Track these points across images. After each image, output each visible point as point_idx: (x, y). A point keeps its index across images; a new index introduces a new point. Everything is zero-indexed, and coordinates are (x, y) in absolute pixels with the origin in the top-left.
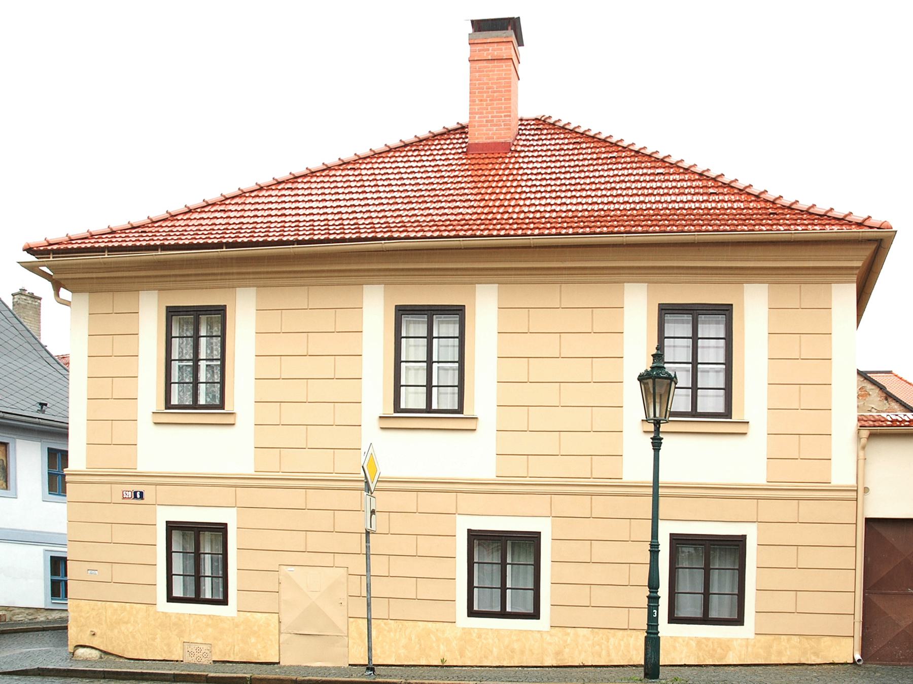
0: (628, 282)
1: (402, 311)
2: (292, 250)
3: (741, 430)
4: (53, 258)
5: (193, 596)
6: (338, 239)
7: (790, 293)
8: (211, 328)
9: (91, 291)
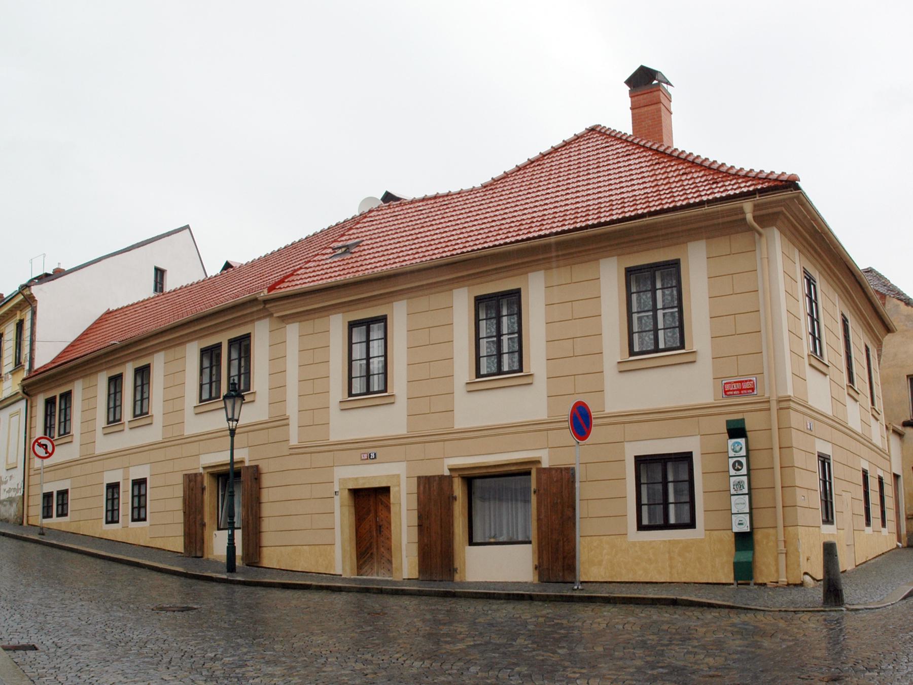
0: (455, 288)
1: (352, 325)
2: (586, 234)
3: (390, 401)
4: (759, 197)
5: (662, 522)
6: (697, 203)
7: (423, 302)
8: (639, 285)
9: (708, 238)
